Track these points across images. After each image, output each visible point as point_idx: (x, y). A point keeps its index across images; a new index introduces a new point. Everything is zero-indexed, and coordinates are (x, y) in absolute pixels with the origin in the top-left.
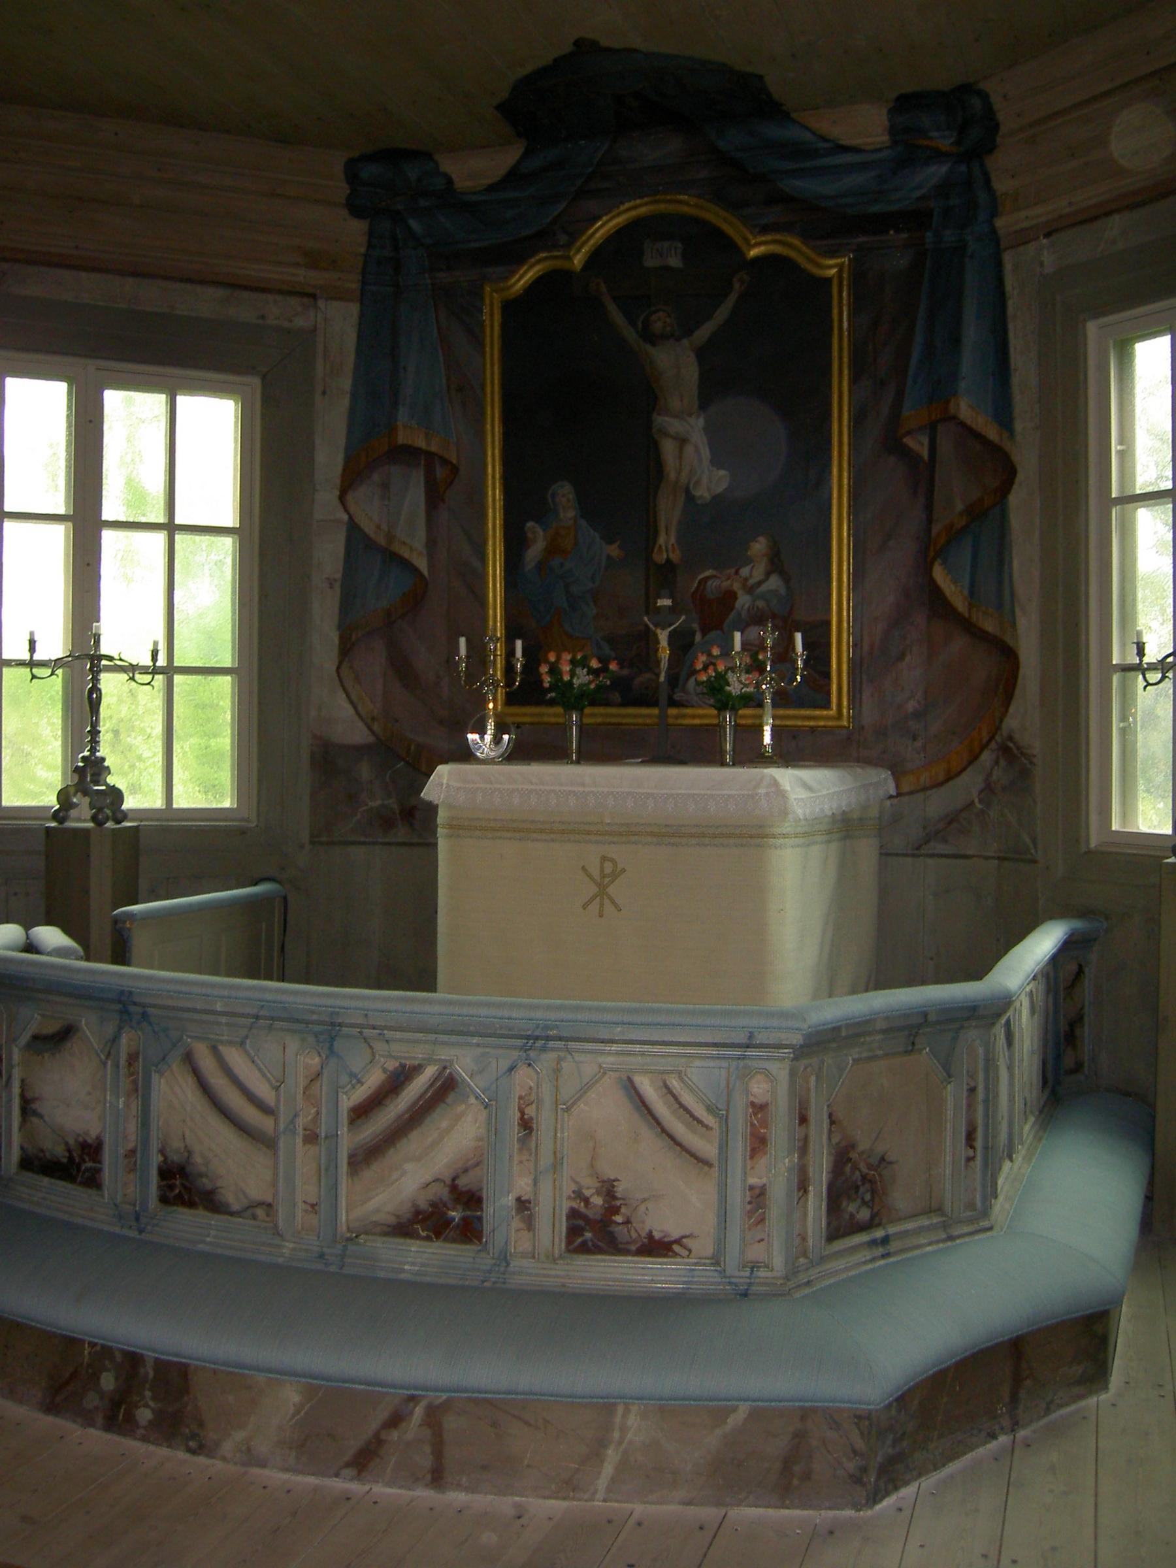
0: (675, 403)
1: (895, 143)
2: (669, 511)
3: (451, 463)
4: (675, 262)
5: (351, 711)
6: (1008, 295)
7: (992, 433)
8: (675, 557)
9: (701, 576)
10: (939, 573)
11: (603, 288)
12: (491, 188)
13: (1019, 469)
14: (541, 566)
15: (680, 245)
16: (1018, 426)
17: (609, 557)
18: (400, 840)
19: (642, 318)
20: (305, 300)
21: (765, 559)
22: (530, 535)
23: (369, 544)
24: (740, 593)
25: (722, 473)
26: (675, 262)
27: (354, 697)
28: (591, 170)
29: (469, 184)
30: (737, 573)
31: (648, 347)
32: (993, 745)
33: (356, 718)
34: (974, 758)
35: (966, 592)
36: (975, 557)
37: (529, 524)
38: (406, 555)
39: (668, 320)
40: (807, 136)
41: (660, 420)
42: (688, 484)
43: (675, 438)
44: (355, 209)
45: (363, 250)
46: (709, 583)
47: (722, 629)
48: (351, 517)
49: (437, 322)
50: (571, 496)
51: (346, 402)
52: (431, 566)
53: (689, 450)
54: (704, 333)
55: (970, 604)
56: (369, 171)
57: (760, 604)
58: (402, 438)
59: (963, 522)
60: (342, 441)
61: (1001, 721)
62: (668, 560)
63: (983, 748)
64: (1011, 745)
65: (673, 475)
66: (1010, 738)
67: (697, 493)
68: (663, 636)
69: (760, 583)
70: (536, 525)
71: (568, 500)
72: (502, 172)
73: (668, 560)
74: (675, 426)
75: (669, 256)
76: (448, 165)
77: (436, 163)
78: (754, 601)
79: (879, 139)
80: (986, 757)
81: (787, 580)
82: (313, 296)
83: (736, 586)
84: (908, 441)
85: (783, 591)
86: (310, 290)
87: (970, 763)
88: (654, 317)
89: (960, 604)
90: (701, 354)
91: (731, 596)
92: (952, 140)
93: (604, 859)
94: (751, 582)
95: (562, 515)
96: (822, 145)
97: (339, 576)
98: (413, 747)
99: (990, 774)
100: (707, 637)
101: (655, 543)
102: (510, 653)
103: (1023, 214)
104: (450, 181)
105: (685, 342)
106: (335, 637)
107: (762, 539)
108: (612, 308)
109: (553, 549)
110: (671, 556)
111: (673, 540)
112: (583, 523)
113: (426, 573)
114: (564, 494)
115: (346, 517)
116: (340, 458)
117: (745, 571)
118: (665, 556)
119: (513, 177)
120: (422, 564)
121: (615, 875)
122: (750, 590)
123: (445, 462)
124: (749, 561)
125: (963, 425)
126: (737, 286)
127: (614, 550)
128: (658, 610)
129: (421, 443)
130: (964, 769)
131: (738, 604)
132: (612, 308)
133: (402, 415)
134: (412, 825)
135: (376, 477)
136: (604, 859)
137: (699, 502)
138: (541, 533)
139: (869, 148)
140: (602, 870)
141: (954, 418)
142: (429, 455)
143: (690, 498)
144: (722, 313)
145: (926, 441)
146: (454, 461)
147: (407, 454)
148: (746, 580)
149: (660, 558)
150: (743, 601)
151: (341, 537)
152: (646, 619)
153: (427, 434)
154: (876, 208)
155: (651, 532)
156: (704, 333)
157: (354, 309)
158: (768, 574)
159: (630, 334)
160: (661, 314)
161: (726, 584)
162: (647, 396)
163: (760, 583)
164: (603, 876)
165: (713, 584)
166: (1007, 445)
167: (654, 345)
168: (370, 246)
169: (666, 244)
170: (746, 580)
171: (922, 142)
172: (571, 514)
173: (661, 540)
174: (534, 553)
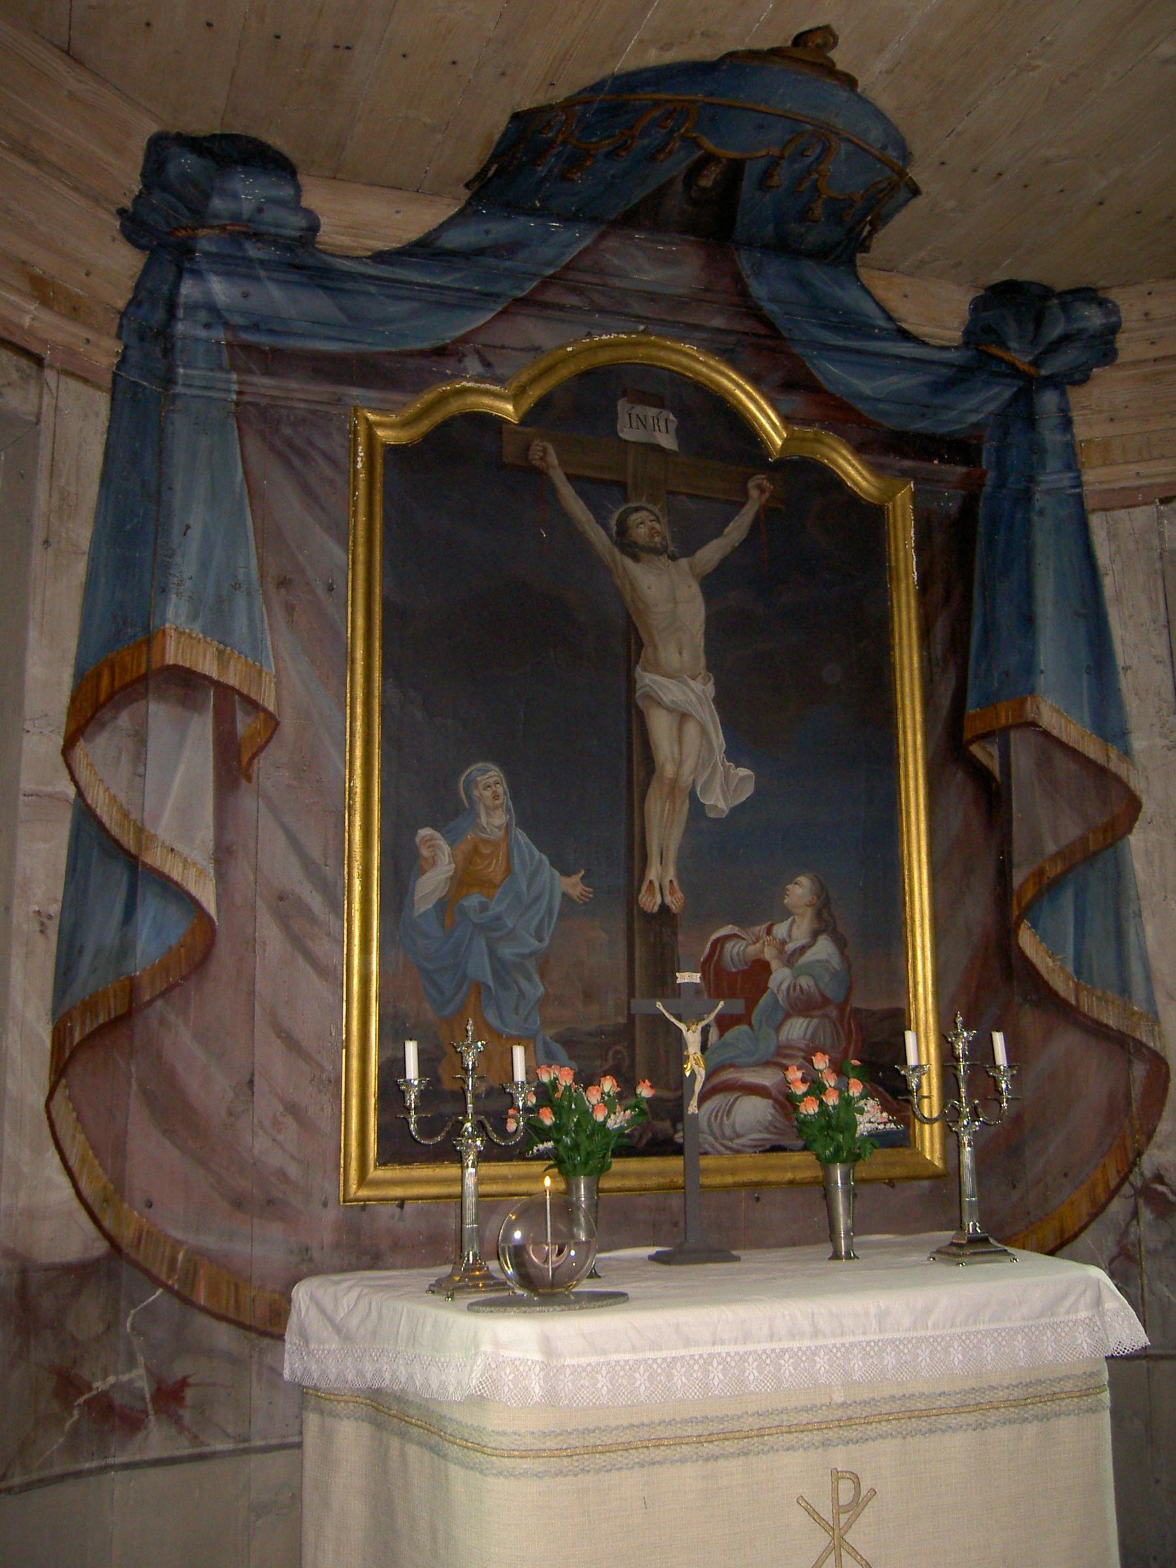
0: (670, 655)
1: (966, 344)
2: (665, 828)
3: (265, 710)
4: (668, 441)
5: (69, 1191)
6: (1102, 570)
7: (1092, 749)
8: (675, 902)
9: (713, 937)
10: (1027, 941)
11: (553, 459)
12: (380, 257)
13: (1144, 799)
14: (444, 906)
15: (672, 417)
16: (1138, 743)
17: (565, 895)
18: (152, 1455)
19: (616, 516)
20: (24, 363)
21: (809, 912)
22: (425, 852)
23: (114, 848)
24: (774, 964)
25: (743, 772)
26: (668, 441)
27: (73, 1161)
28: (551, 272)
29: (346, 241)
30: (769, 932)
31: (628, 562)
32: (1127, 1189)
33: (76, 1203)
34: (1098, 1210)
35: (1070, 969)
36: (1080, 922)
37: (425, 832)
38: (176, 875)
39: (657, 526)
40: (869, 308)
41: (647, 679)
42: (694, 788)
43: (669, 710)
44: (134, 226)
45: (121, 304)
46: (728, 946)
47: (750, 1024)
48: (80, 793)
49: (244, 461)
50: (500, 789)
51: (81, 568)
52: (223, 896)
53: (691, 729)
54: (711, 554)
55: (1077, 985)
56: (187, 163)
57: (805, 982)
58: (173, 653)
59: (1059, 868)
60: (71, 644)
61: (1139, 1154)
62: (664, 908)
63: (1112, 1194)
64: (1161, 1188)
65: (669, 770)
66: (1159, 1179)
67: (707, 801)
68: (692, 1038)
69: (803, 950)
70: (438, 835)
71: (496, 797)
72: (413, 235)
73: (664, 908)
74: (671, 691)
75: (651, 428)
76: (315, 197)
77: (298, 189)
78: (795, 978)
79: (948, 334)
80: (1118, 1207)
81: (840, 942)
82: (38, 361)
83: (769, 954)
84: (975, 749)
85: (836, 963)
86: (35, 348)
87: (1094, 1216)
88: (635, 517)
89: (1062, 985)
90: (712, 584)
91: (761, 969)
92: (1030, 358)
93: (836, 1476)
94: (790, 947)
95: (483, 820)
96: (882, 323)
97: (55, 909)
98: (181, 1256)
99: (1125, 1233)
100: (728, 1035)
101: (641, 881)
102: (392, 1068)
103: (1134, 468)
104: (314, 228)
105: (683, 562)
106: (45, 1033)
107: (803, 880)
108: (568, 493)
109: (465, 879)
110: (668, 900)
111: (671, 874)
112: (522, 837)
113: (212, 909)
114: (488, 784)
115: (71, 791)
116: (66, 678)
117: (781, 930)
118: (659, 901)
119: (424, 250)
120: (206, 895)
121: (857, 1505)
122: (790, 960)
123: (253, 705)
124: (786, 913)
125: (1046, 734)
126: (754, 493)
127: (574, 885)
128: (678, 990)
129: (208, 666)
130: (1084, 1227)
131: (772, 983)
132: (568, 493)
133: (175, 613)
134: (178, 1422)
135: (124, 719)
136: (836, 1476)
137: (712, 815)
138: (447, 849)
139: (933, 342)
140: (835, 1500)
141: (1034, 724)
142: (224, 691)
143: (697, 808)
144: (736, 531)
145: (995, 751)
146: (271, 708)
147: (186, 684)
148: (783, 943)
149: (650, 902)
150: (780, 977)
151: (62, 833)
152: (659, 1005)
153: (221, 653)
154: (920, 426)
155: (636, 857)
156: (711, 554)
157: (102, 402)
158: (815, 935)
159: (599, 537)
160: (644, 514)
161: (752, 949)
162: (627, 642)
163: (803, 950)
164: (839, 1509)
165: (732, 949)
166: (1116, 765)
167: (636, 558)
168: (135, 302)
169: (652, 412)
170: (783, 943)
171: (995, 350)
172: (500, 819)
173: (653, 874)
174: (430, 885)
